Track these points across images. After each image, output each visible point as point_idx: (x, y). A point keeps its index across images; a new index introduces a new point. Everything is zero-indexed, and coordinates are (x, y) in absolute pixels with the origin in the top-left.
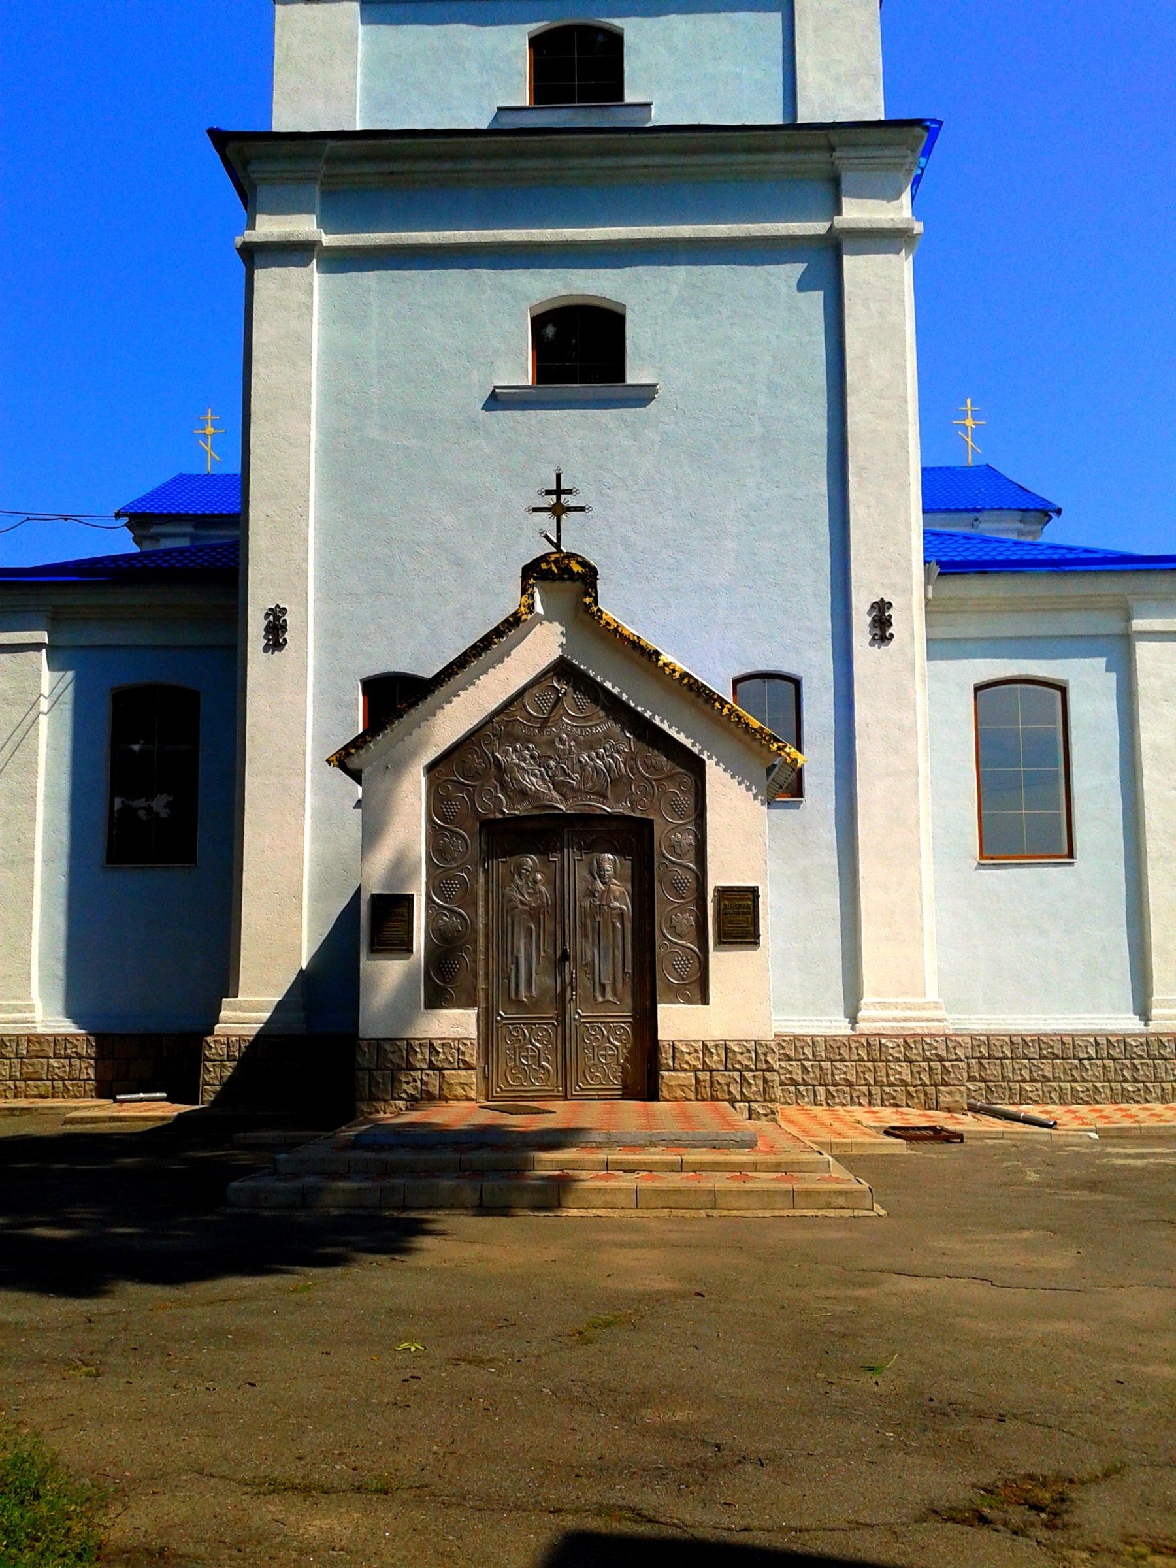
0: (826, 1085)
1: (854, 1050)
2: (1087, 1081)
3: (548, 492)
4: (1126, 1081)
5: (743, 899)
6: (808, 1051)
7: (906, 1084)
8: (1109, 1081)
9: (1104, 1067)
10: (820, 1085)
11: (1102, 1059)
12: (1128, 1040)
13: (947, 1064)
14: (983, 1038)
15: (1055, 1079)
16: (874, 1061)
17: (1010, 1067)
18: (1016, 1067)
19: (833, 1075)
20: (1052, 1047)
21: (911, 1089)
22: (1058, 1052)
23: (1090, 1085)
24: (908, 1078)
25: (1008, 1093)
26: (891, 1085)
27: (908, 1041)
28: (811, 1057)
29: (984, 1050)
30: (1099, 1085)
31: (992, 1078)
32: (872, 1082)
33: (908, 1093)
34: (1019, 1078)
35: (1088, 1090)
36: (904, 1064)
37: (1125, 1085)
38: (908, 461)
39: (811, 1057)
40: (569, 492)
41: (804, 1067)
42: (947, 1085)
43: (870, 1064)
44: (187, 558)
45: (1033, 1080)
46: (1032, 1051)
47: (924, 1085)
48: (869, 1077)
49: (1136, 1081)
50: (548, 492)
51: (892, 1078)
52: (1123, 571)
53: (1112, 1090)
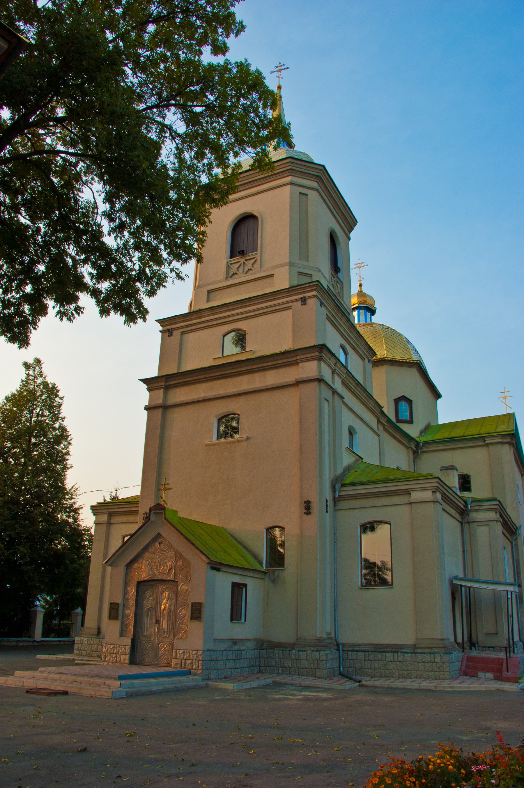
4: (403, 670)
9: (396, 664)
15: (379, 668)
26: (302, 668)
30: (394, 671)
33: (307, 671)
37: (404, 672)
42: (319, 669)
43: (295, 660)
45: (371, 668)
47: (312, 668)
48: (295, 665)
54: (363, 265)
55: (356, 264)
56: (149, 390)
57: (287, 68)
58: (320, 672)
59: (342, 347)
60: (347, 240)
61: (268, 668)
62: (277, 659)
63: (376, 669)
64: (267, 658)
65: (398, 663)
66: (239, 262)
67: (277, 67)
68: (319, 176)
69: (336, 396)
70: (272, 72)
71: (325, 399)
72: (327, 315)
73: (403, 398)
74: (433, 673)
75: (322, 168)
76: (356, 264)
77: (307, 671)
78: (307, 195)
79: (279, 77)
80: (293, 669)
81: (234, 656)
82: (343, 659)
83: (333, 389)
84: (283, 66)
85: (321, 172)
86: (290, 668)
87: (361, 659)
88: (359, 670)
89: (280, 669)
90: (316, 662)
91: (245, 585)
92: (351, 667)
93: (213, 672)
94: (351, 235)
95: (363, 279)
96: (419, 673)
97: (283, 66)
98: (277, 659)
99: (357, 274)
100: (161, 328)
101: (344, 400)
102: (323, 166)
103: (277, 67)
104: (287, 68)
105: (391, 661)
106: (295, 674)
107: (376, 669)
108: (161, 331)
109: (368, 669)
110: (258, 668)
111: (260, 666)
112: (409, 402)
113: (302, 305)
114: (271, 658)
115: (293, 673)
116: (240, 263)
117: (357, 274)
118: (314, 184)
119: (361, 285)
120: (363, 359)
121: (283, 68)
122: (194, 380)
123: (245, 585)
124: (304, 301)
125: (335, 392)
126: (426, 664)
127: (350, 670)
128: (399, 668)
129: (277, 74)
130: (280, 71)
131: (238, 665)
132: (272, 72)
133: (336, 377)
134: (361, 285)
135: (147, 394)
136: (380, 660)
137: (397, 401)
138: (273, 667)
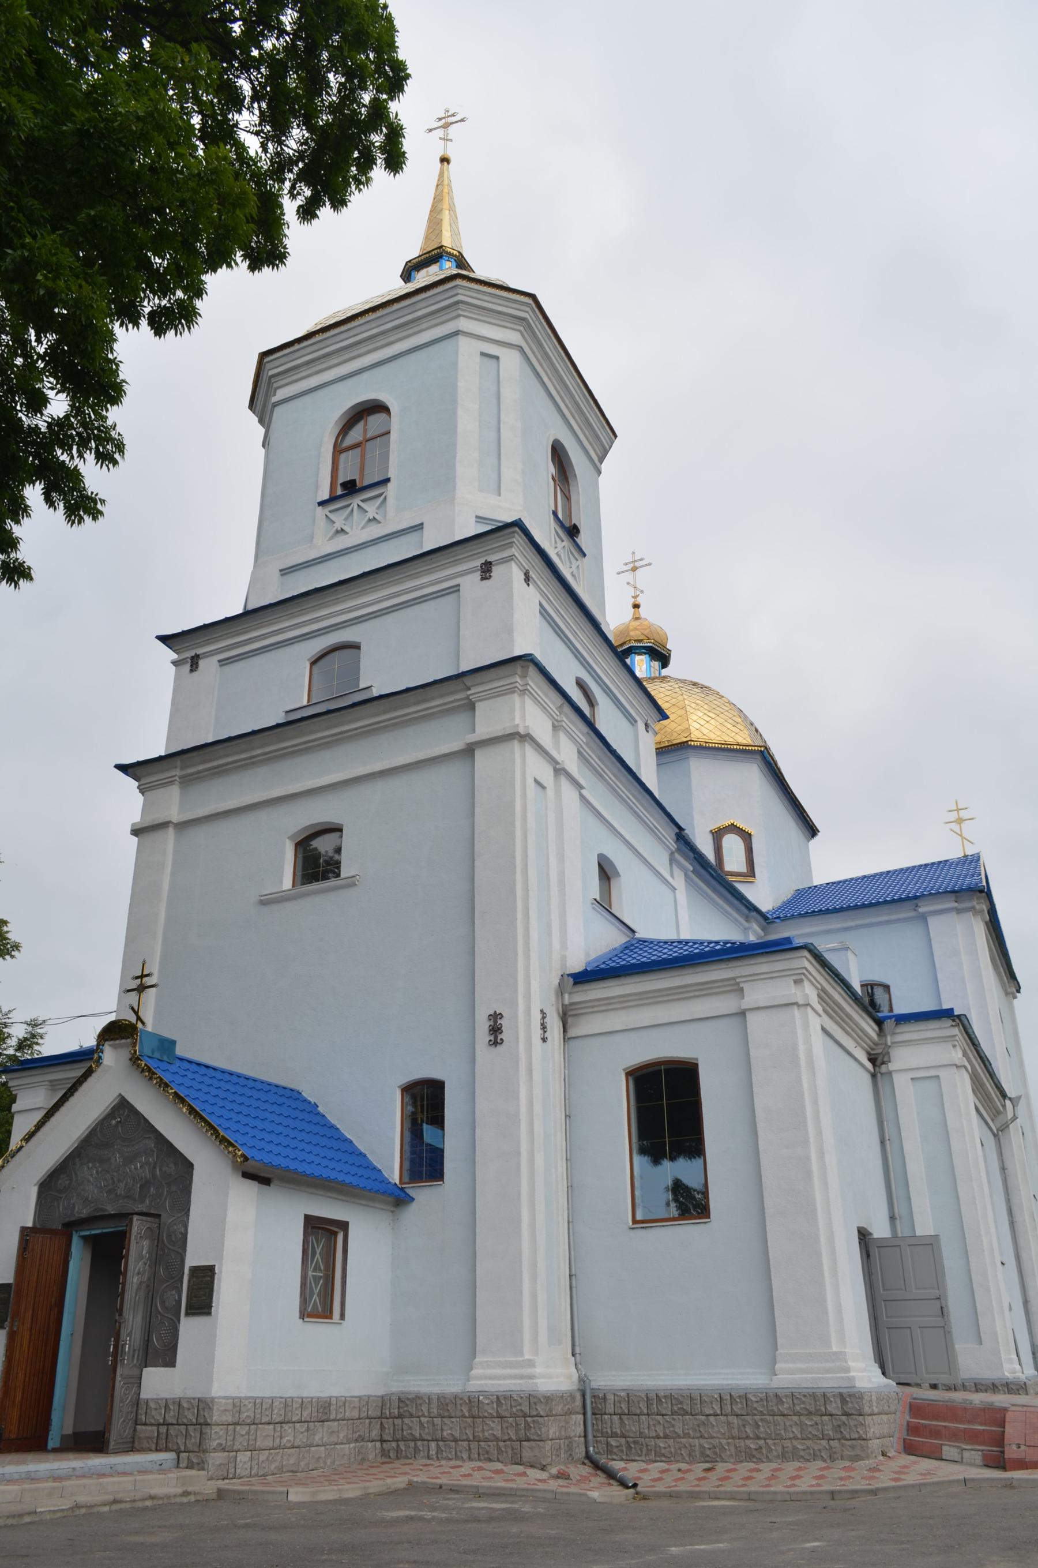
0: (437, 1440)
1: (458, 1406)
2: (713, 1438)
3: (137, 978)
4: (748, 1437)
5: (204, 1277)
6: (425, 1408)
7: (497, 1439)
8: (733, 1438)
9: (729, 1423)
10: (433, 1440)
11: (726, 1415)
12: (749, 1396)
13: (529, 1419)
14: (622, 1394)
15: (687, 1435)
16: (474, 1417)
17: (646, 1423)
18: (788, 1424)
19: (442, 1430)
20: (804, 1403)
21: (501, 1444)
22: (688, 1408)
23: (716, 1442)
24: (498, 1434)
25: (644, 1449)
26: (486, 1440)
27: (499, 1399)
28: (426, 1414)
29: (624, 1406)
30: (724, 1442)
31: (631, 1435)
32: (471, 1438)
33: (499, 1448)
34: (654, 1434)
35: (714, 1447)
36: (496, 1420)
37: (748, 1442)
38: (515, 901)
39: (426, 1414)
40: (148, 975)
41: (421, 1424)
42: (528, 1440)
43: (469, 1420)
44: (691, 947)
45: (666, 1437)
46: (834, 1407)
47: (510, 1439)
48: (469, 1432)
49: (758, 1438)
50: (137, 978)
51: (445, 1434)
52: (729, 960)
53: (736, 1447)
54: (641, 563)
55: (625, 564)
56: (142, 791)
57: (462, 120)
58: (531, 1448)
59: (580, 684)
60: (596, 474)
61: (402, 1444)
62: (424, 1420)
63: (679, 1437)
64: (400, 1416)
65: (734, 1420)
66: (349, 505)
67: (440, 119)
68: (524, 319)
69: (564, 782)
70: (430, 130)
71: (536, 780)
72: (541, 605)
73: (733, 828)
74: (824, 1443)
75: (530, 301)
76: (625, 564)
77: (499, 1448)
78: (497, 358)
79: (445, 139)
80: (465, 1444)
81: (305, 1414)
82: (594, 1414)
83: (557, 763)
84: (453, 115)
85: (528, 309)
86: (456, 1441)
87: (638, 1411)
88: (634, 1442)
89: (433, 1444)
90: (521, 1421)
91: (344, 1226)
92: (614, 1435)
93: (243, 1457)
94: (604, 466)
95: (642, 592)
96: (787, 1444)
97: (453, 115)
98: (424, 1420)
99: (628, 583)
100: (174, 656)
101: (583, 791)
102: (533, 297)
103: (440, 119)
104: (462, 120)
105: (715, 1415)
106: (470, 1459)
107: (679, 1437)
108: (175, 663)
109: (796, 1438)
110: (378, 1444)
111: (382, 1441)
112: (747, 837)
113: (483, 579)
114: (411, 1416)
115: (465, 1456)
116: (350, 509)
117: (628, 583)
118: (514, 337)
119: (636, 606)
120: (633, 721)
121: (453, 119)
122: (244, 759)
123: (344, 1226)
124: (486, 570)
125: (559, 771)
126: (803, 1418)
127: (614, 1443)
128: (735, 1432)
129: (440, 133)
130: (446, 126)
131: (317, 1438)
132: (430, 130)
133: (563, 738)
134: (636, 606)
135: (140, 798)
136: (686, 1413)
137: (718, 835)
138: (415, 1440)
